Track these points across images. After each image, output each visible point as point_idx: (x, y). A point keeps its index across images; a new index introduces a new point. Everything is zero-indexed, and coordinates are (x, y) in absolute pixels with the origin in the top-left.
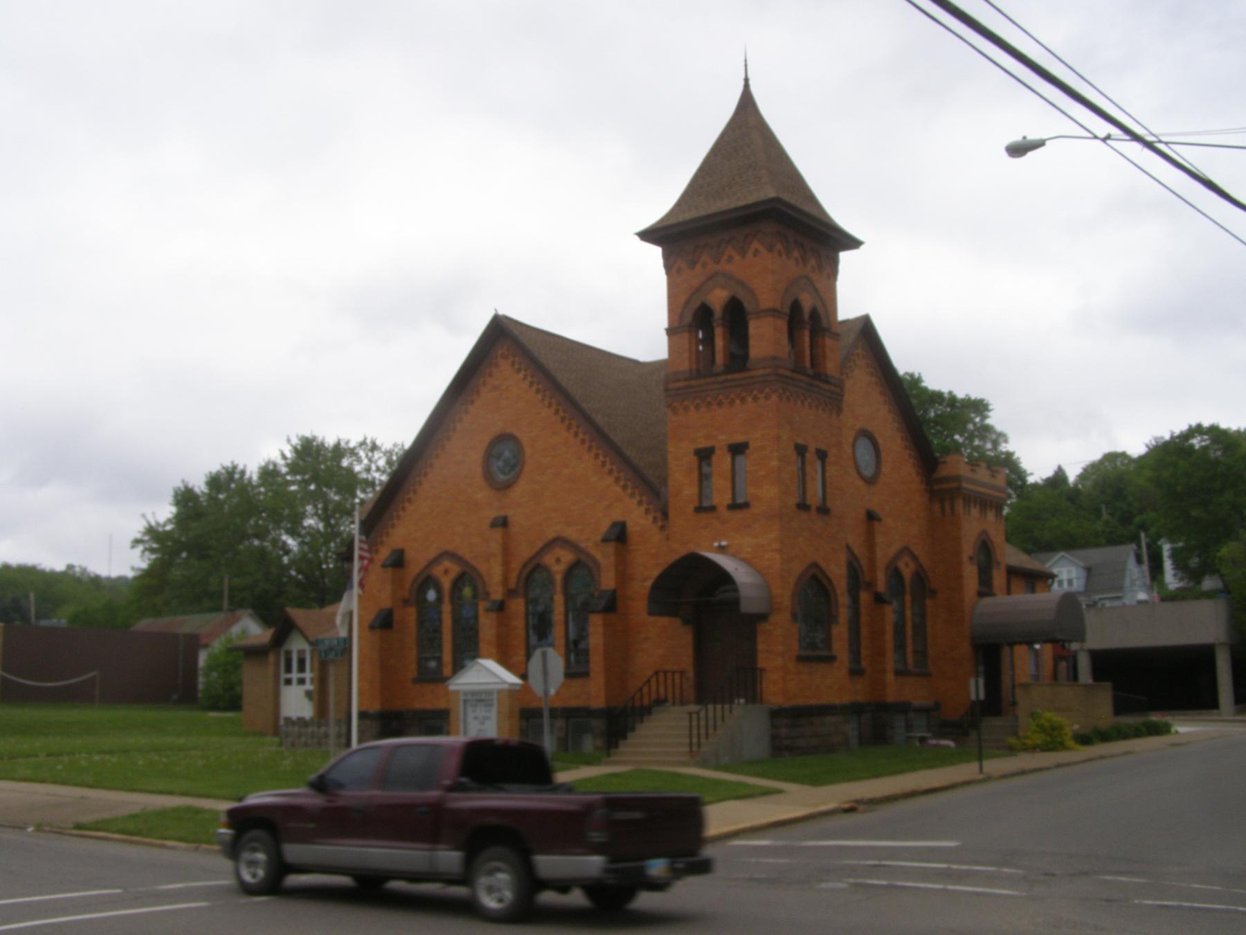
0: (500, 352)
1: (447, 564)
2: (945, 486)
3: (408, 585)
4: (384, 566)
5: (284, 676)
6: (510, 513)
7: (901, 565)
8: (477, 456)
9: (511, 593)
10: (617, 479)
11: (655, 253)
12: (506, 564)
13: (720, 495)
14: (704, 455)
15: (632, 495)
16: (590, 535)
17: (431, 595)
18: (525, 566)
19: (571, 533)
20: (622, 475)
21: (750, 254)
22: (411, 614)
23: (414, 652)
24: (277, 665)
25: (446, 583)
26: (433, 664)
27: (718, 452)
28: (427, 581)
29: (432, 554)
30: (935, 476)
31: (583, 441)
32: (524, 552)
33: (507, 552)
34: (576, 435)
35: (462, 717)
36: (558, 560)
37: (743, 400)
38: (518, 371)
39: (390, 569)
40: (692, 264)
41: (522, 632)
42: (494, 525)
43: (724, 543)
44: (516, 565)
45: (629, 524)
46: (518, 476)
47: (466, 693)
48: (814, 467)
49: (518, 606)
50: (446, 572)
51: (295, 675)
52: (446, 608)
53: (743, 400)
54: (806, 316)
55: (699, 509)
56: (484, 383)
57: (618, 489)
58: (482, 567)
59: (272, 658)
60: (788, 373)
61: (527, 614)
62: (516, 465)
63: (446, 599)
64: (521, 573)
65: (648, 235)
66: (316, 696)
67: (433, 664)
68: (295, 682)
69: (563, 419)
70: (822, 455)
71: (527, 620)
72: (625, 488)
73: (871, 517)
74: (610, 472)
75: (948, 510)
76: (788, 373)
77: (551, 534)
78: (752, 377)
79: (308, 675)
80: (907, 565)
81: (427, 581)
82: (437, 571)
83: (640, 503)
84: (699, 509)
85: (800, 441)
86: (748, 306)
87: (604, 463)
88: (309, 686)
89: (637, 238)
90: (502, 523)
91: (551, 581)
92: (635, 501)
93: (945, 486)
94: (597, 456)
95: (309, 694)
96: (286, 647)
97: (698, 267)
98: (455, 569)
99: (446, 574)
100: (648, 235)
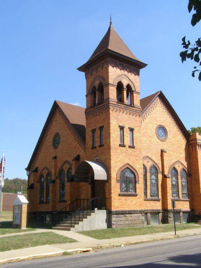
2: (192, 142)
6: (57, 155)
7: (176, 166)
9: (57, 178)
11: (83, 74)
12: (56, 169)
13: (127, 141)
14: (94, 131)
17: (43, 180)
18: (59, 170)
21: (104, 69)
22: (39, 185)
23: (39, 196)
26: (42, 199)
27: (97, 130)
28: (42, 176)
30: (190, 139)
33: (56, 166)
37: (102, 113)
39: (75, 161)
40: (91, 75)
41: (59, 189)
43: (97, 158)
45: (80, 155)
48: (127, 133)
49: (58, 181)
50: (45, 173)
52: (45, 183)
53: (102, 113)
54: (125, 86)
55: (120, 145)
57: (78, 145)
60: (115, 103)
61: (60, 183)
63: (45, 180)
64: (59, 172)
65: (80, 69)
70: (132, 130)
71: (60, 185)
73: (162, 151)
75: (194, 150)
76: (115, 103)
78: (104, 105)
80: (179, 166)
84: (120, 145)
85: (121, 125)
86: (103, 84)
89: (78, 70)
90: (55, 158)
91: (64, 173)
92: (82, 148)
93: (192, 142)
97: (93, 76)
99: (45, 173)
100: (80, 69)
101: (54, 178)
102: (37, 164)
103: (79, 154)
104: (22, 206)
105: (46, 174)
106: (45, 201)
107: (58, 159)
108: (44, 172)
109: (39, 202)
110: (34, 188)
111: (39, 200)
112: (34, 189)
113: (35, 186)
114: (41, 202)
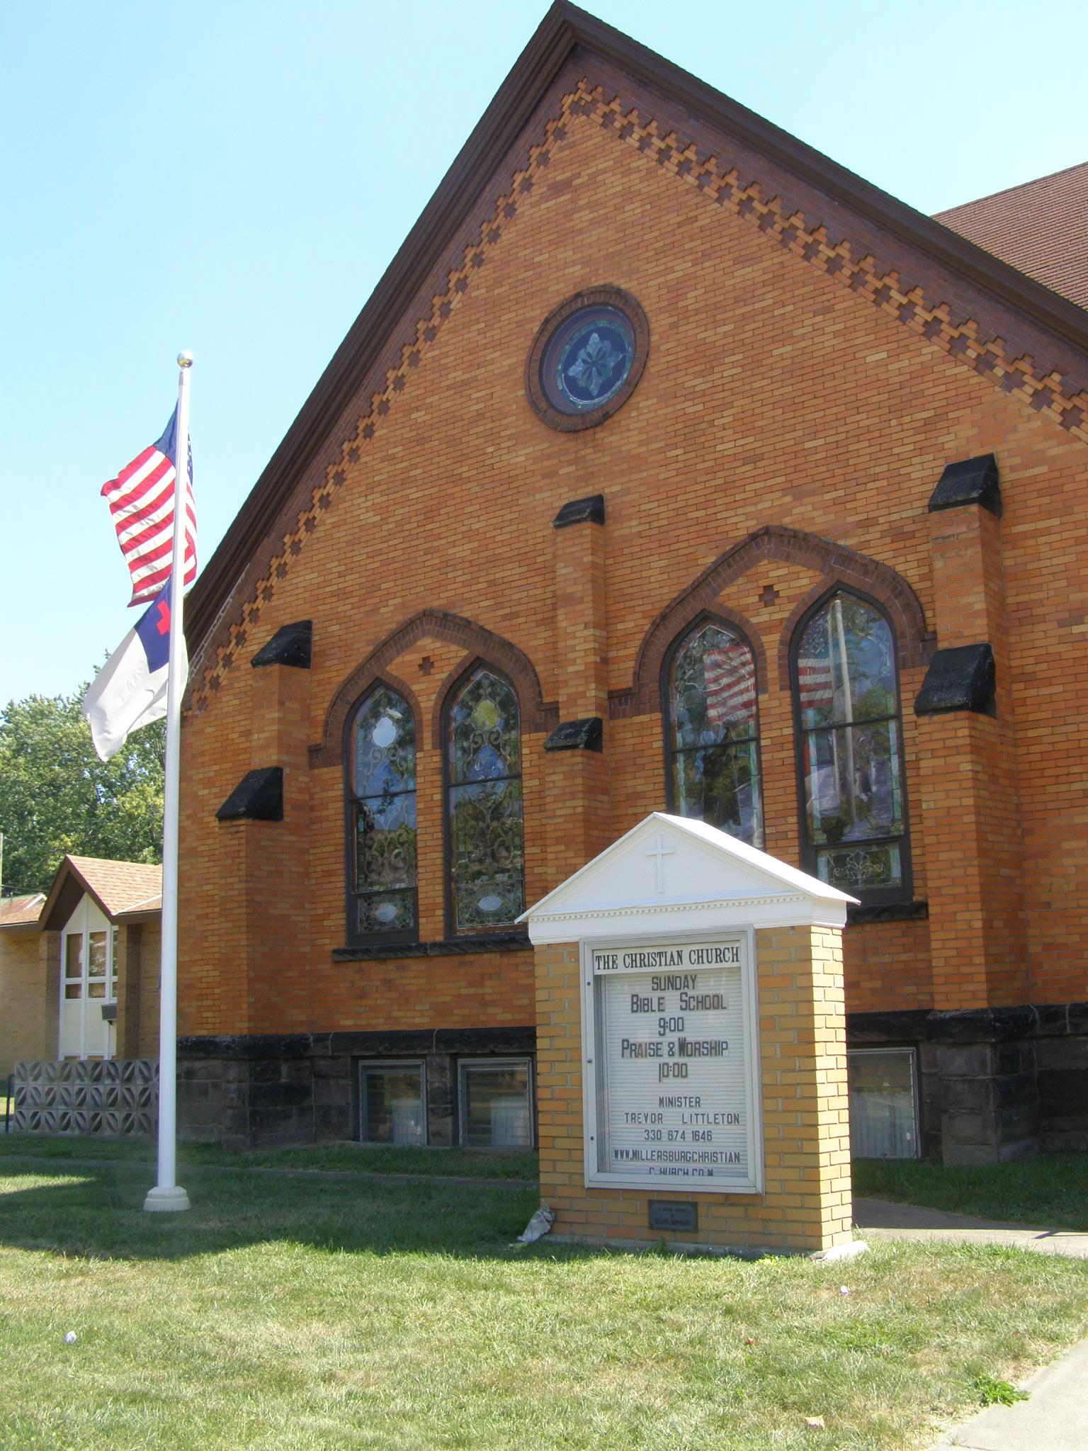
0: (569, 100)
1: (428, 644)
3: (320, 713)
4: (257, 662)
5: (65, 981)
6: (609, 489)
8: (510, 360)
9: (619, 700)
10: (956, 346)
12: (604, 621)
15: (1012, 381)
16: (879, 504)
19: (810, 515)
20: (969, 330)
23: (340, 882)
24: (55, 958)
25: (427, 694)
29: (390, 617)
31: (833, 265)
32: (657, 581)
34: (810, 252)
35: (589, 1051)
36: (769, 595)
38: (624, 132)
39: (276, 668)
42: (567, 517)
44: (633, 625)
46: (632, 387)
47: (605, 952)
50: (426, 665)
51: (84, 980)
56: (527, 185)
58: (532, 641)
59: (43, 948)
61: (670, 755)
62: (625, 377)
64: (647, 644)
66: (122, 1015)
67: (388, 911)
68: (84, 991)
69: (765, 222)
72: (983, 364)
74: (931, 329)
77: (743, 524)
79: (109, 979)
81: (373, 689)
82: (402, 665)
83: (1042, 399)
87: (906, 312)
88: (109, 999)
92: (1023, 395)
94: (881, 295)
95: (108, 1013)
96: (71, 928)
98: (451, 655)
101: (598, 707)
102: (297, 588)
103: (307, 618)
104: (808, 948)
105: (442, 675)
106: (431, 928)
107: (624, 528)
108: (411, 658)
109: (340, 941)
110: (287, 807)
111: (338, 920)
112: (287, 819)
113: (290, 792)
114: (371, 944)
